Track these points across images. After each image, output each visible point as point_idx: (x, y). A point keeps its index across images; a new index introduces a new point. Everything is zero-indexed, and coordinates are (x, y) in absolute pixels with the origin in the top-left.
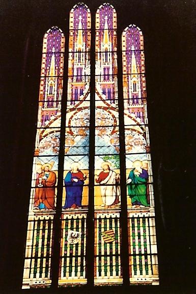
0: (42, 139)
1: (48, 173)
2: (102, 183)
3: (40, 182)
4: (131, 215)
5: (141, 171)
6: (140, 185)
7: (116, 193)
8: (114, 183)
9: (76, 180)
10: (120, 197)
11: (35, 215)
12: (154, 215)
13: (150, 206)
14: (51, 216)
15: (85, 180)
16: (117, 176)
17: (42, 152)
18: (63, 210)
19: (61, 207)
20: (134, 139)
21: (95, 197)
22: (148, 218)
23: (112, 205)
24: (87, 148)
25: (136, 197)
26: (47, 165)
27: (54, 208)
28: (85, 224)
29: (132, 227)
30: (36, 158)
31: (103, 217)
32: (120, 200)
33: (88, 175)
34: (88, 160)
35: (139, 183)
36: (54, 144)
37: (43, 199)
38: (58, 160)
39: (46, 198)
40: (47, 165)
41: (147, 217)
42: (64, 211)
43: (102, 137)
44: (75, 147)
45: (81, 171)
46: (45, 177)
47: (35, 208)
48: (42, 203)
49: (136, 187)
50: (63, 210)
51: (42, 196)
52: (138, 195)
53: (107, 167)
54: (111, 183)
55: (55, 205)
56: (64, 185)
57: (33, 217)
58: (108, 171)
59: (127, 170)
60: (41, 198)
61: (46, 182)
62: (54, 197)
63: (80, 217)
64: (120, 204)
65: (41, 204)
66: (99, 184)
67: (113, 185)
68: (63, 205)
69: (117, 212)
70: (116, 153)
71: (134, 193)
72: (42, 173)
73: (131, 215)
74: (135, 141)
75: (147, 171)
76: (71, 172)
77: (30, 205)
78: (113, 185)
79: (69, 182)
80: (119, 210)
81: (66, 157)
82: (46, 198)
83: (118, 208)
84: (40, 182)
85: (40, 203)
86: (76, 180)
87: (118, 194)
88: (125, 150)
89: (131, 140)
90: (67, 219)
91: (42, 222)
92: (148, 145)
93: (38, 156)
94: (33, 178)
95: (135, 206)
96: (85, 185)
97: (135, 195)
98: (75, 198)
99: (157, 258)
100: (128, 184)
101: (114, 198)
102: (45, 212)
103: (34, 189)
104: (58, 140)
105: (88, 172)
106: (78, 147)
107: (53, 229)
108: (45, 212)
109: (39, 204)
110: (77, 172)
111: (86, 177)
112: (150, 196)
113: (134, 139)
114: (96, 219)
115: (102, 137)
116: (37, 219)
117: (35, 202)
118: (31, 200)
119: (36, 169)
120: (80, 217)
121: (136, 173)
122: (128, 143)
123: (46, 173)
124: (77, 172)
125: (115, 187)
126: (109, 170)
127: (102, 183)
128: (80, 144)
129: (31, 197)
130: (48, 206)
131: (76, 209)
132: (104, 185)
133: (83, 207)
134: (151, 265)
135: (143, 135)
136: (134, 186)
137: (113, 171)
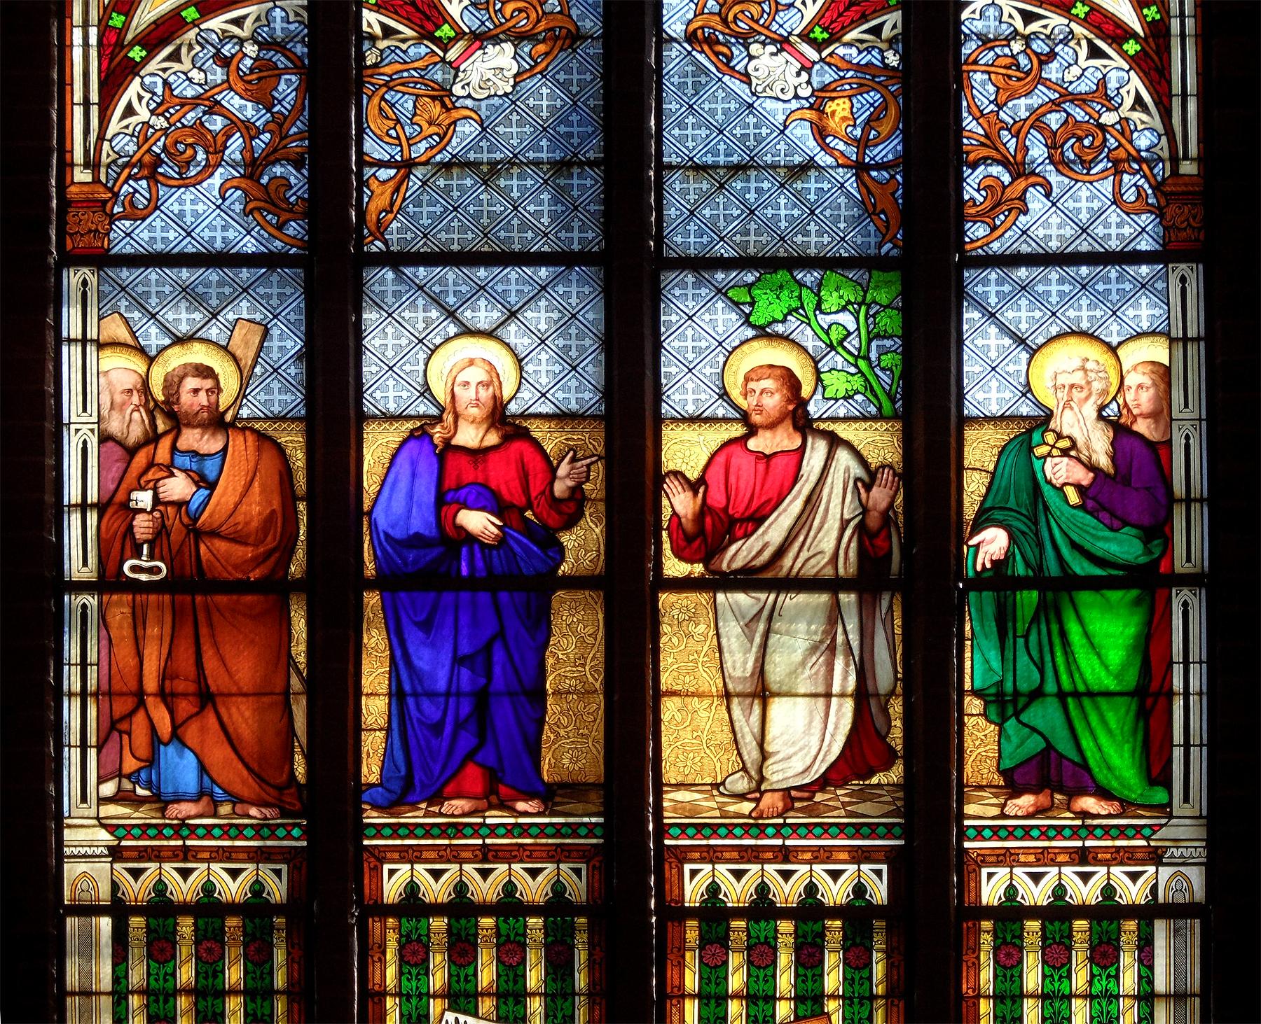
0: (133, 69)
1: (210, 444)
2: (740, 554)
3: (142, 526)
4: (991, 891)
5: (1099, 447)
6: (1084, 597)
7: (864, 672)
8: (848, 566)
9: (477, 521)
10: (896, 707)
11: (116, 853)
12: (1199, 894)
13: (1165, 809)
14: (266, 871)
15: (571, 521)
16: (879, 496)
17: (136, 215)
18: (373, 817)
19: (356, 792)
20: (1041, 96)
21: (670, 709)
22: (1148, 913)
23: (824, 782)
24: (586, 185)
25: (1045, 715)
26: (199, 354)
27: (290, 798)
28: (581, 956)
29: (998, 998)
30: (85, 272)
31: (737, 892)
32: (896, 735)
33: (598, 471)
34: (593, 315)
35: (1081, 567)
36: (248, 130)
37: (185, 707)
38: (294, 307)
39: (206, 698)
40: (199, 354)
41: (1132, 911)
42: (379, 830)
43: (727, 64)
44: (468, 164)
45: (538, 431)
46: (178, 487)
47: (109, 789)
48: (177, 736)
49: (1050, 612)
50: (373, 817)
51: (166, 675)
52: (1062, 696)
53: (774, 402)
54: (816, 566)
55: (300, 770)
56: (370, 568)
57: (101, 872)
58: (781, 440)
59: (970, 434)
60: (166, 696)
61: (196, 532)
62: (286, 693)
63: (534, 889)
64: (895, 774)
65: (169, 754)
66: (698, 569)
67: (832, 585)
68: (371, 771)
69: (860, 855)
70: (577, 239)
71: (1028, 677)
72: (152, 438)
73: (991, 891)
74: (1054, 120)
75: (1158, 452)
76: (438, 433)
77: (72, 756)
78: (832, 585)
79: (416, 541)
80: (889, 831)
81: (382, 279)
82: (206, 698)
83: (871, 812)
84: (142, 526)
85: (155, 740)
86: (477, 521)
87: (885, 674)
88: (957, 213)
89: (1021, 107)
90: (412, 904)
91: (186, 926)
92: (1188, 168)
93: (103, 260)
94: (72, 493)
95: (1026, 801)
96: (575, 583)
97: (1037, 694)
98: (482, 698)
99: (1206, 510)
100: (980, 582)
101: (843, 714)
102: (209, 831)
103: (92, 601)
104: (287, 89)
105: (591, 439)
106: (490, 173)
107: (288, 992)
108: (209, 831)
109: (143, 749)
110: (493, 439)
111: (577, 496)
112: (1178, 704)
113: (1041, 96)
114: (676, 913)
115: (727, 64)
116: (137, 890)
117: (113, 728)
118: (71, 712)
119: (1148, 248)
120: (534, 889)
121: (1060, 470)
122: (990, 140)
123: (191, 438)
124: (493, 439)
125: (848, 599)
126: (802, 422)
127: (740, 554)
128: (513, 135)
129: (72, 678)
130: (230, 771)
131: (495, 818)
132: (748, 579)
133: (550, 795)
134: (1186, 694)
135: (1136, 62)
136: (1028, 599)
137: (835, 441)
